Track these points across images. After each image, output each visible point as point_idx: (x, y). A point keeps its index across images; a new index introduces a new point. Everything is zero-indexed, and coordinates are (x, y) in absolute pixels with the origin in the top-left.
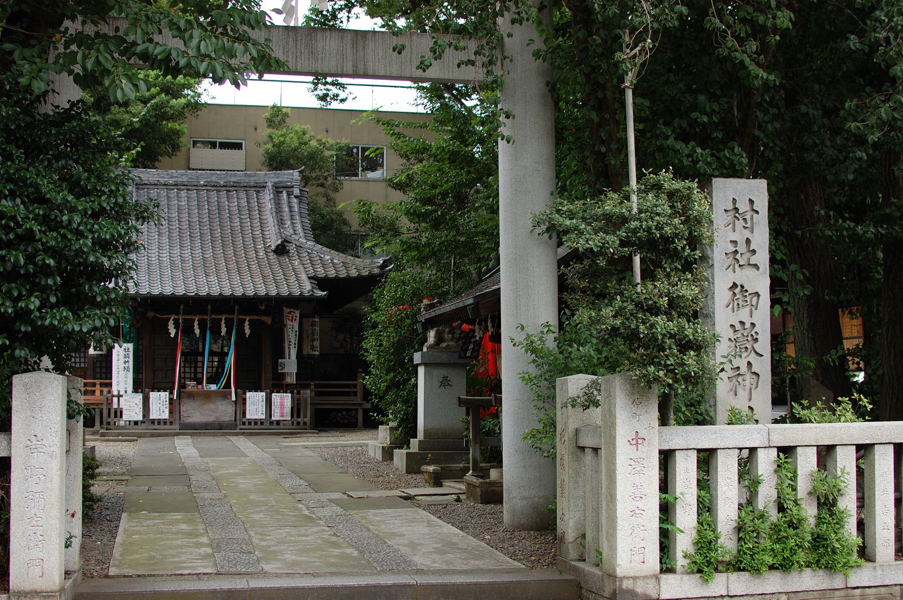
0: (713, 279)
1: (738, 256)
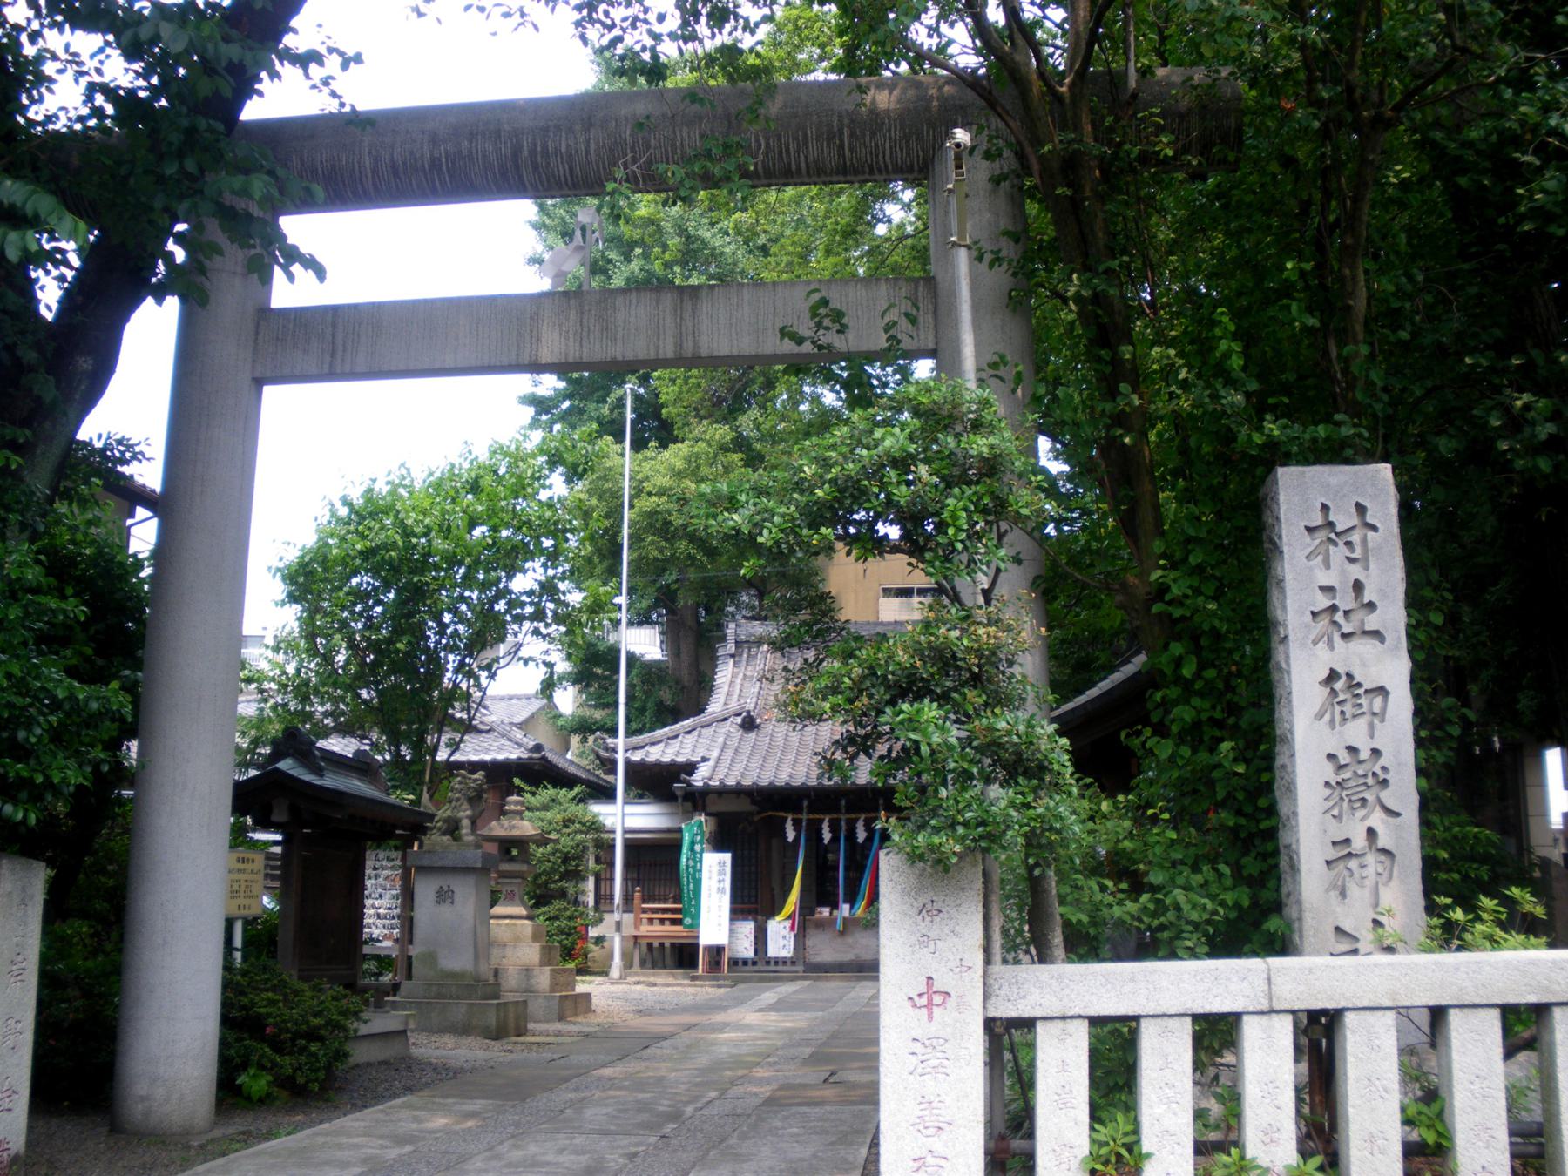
0: (1288, 665)
1: (1339, 617)
